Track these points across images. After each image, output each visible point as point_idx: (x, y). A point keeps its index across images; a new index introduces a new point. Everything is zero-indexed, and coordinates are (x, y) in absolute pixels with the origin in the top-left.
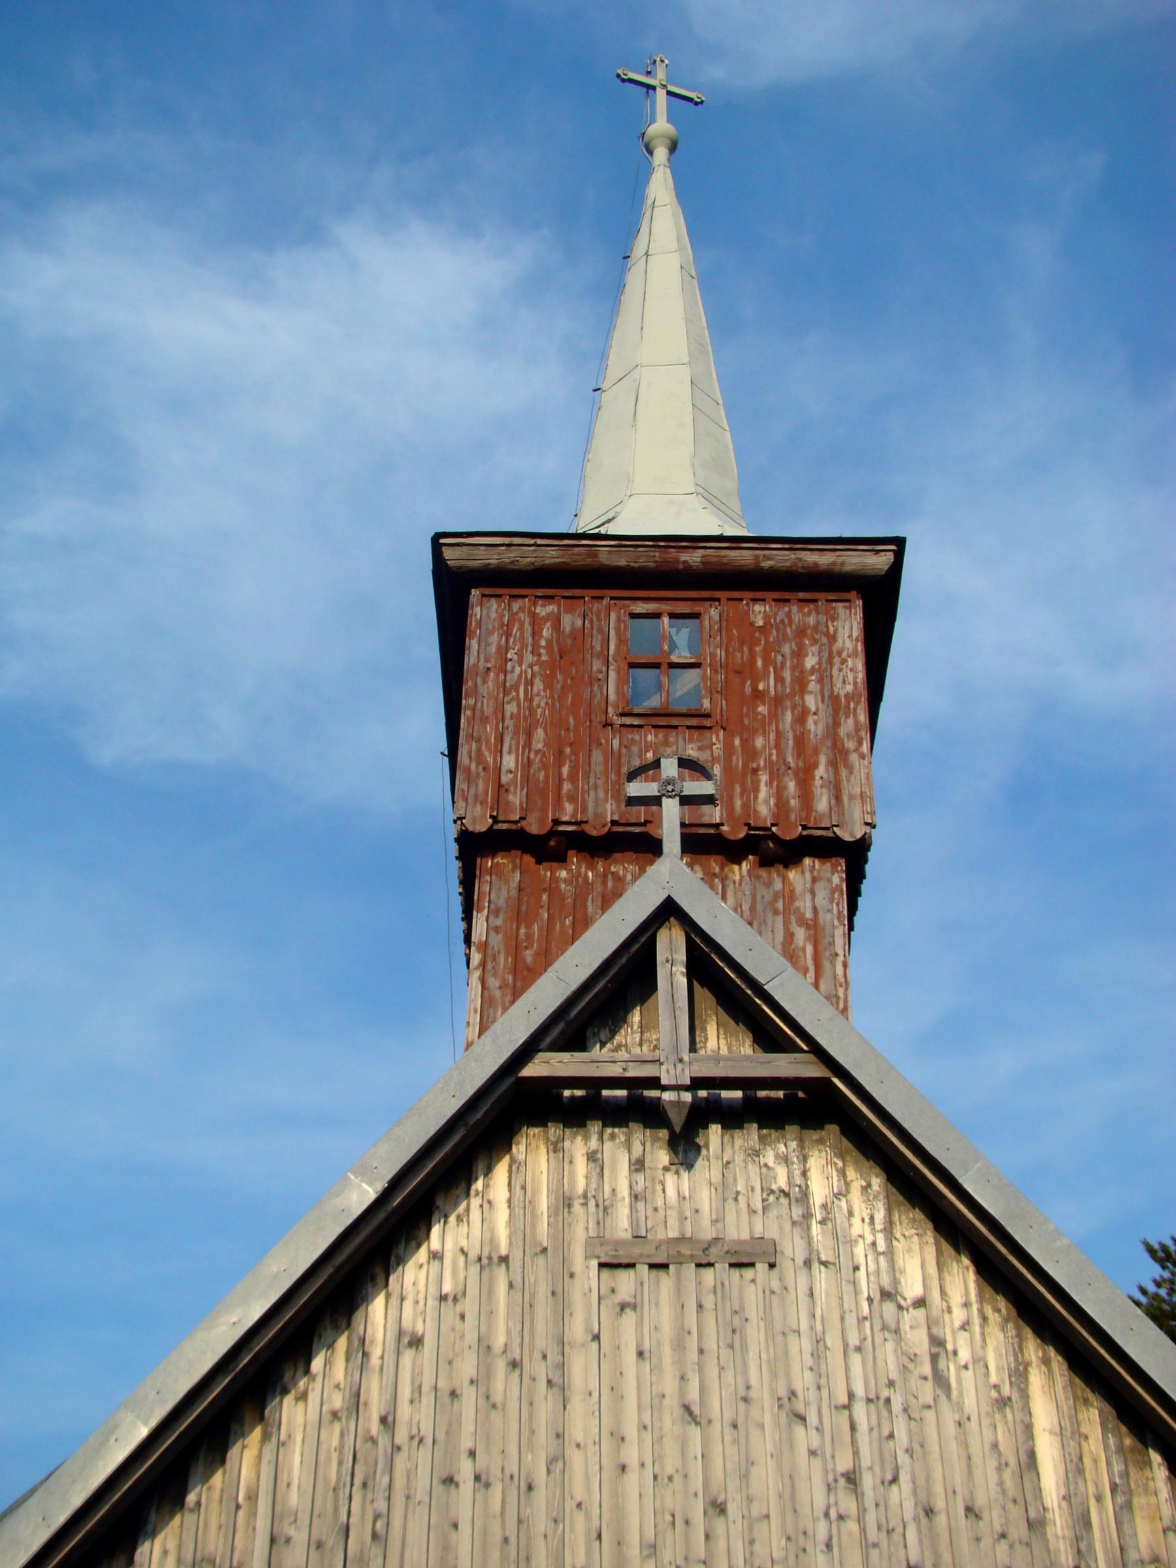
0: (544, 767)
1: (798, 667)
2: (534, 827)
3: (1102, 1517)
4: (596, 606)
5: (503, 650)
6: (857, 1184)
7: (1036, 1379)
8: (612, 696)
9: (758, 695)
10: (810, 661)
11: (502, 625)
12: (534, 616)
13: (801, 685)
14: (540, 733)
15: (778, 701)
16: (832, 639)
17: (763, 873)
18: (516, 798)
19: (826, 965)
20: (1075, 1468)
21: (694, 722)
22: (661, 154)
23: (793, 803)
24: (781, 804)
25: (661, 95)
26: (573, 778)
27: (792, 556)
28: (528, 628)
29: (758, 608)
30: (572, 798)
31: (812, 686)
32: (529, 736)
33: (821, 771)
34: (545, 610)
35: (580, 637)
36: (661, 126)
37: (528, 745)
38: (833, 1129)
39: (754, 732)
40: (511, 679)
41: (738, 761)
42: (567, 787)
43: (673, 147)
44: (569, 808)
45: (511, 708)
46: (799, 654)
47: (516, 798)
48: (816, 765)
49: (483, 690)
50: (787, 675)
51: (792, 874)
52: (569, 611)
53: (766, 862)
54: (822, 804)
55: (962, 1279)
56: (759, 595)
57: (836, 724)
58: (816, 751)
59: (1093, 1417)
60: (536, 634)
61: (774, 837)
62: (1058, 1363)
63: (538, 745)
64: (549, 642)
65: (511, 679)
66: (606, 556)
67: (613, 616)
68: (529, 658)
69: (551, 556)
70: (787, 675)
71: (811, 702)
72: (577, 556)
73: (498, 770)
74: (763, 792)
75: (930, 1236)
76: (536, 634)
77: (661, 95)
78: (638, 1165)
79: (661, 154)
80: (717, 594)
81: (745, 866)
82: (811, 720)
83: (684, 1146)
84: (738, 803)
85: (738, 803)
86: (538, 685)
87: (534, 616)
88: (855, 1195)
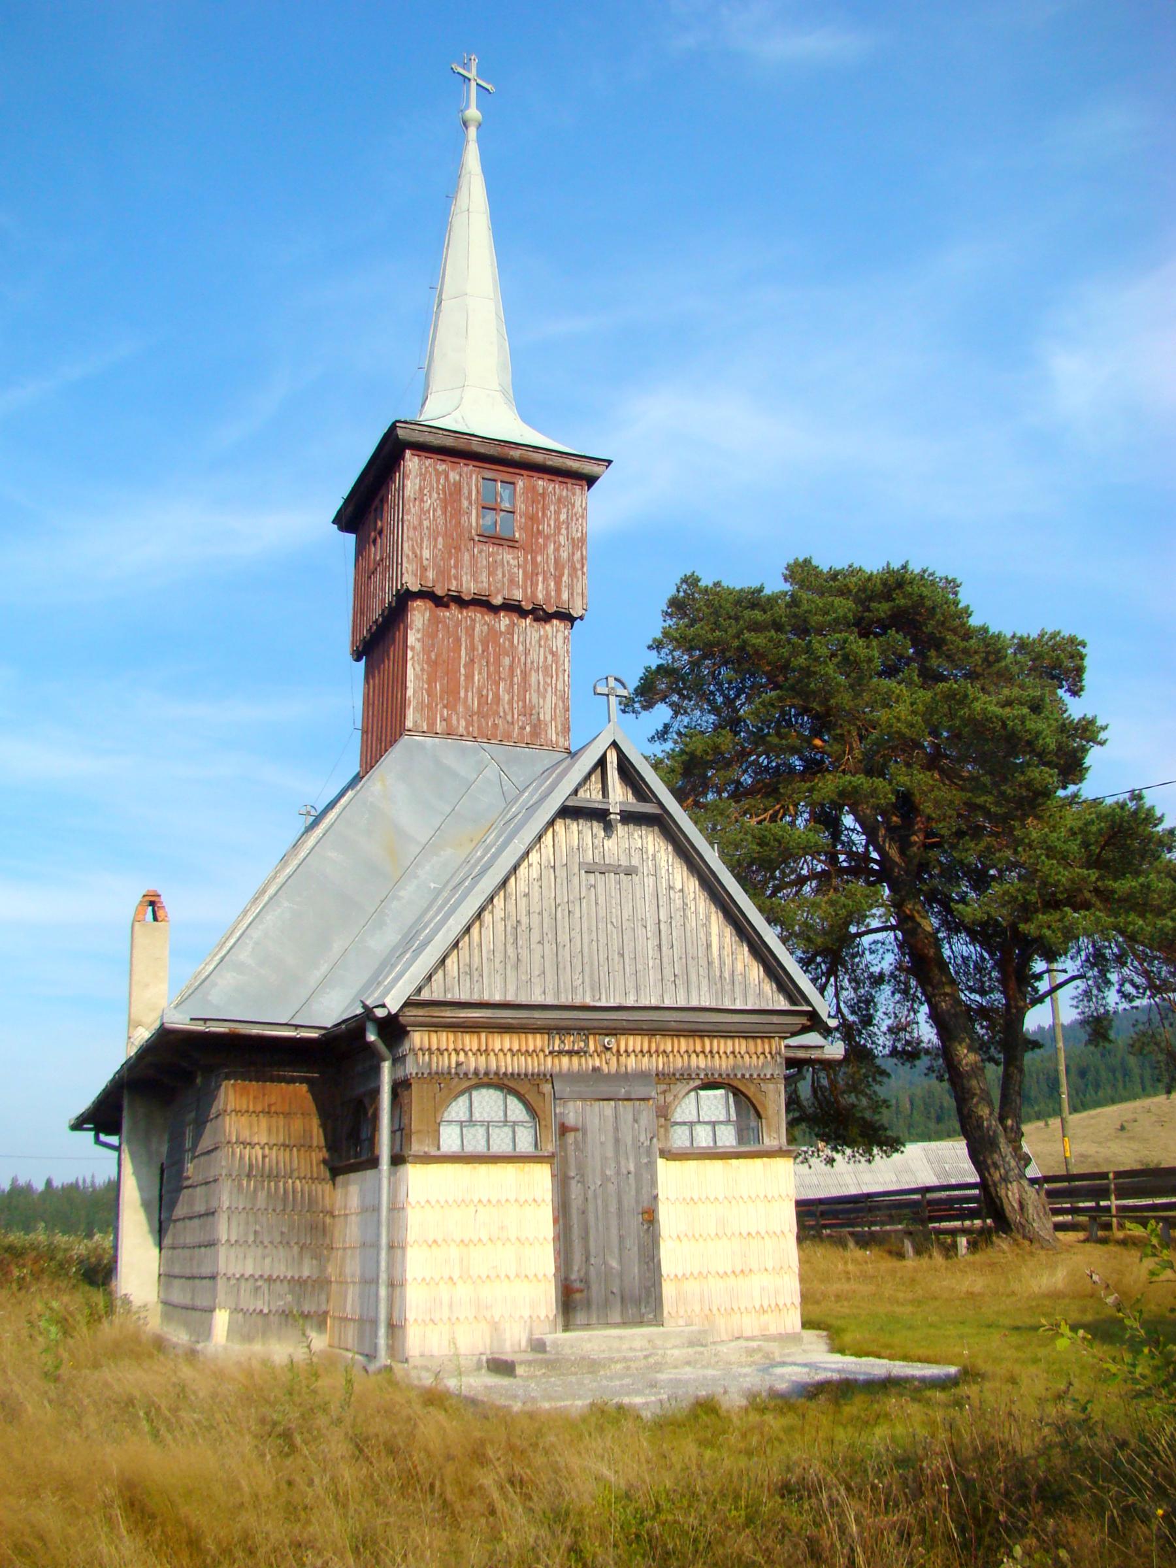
0: (443, 559)
1: (557, 519)
2: (440, 592)
3: (728, 961)
4: (465, 469)
5: (421, 489)
6: (664, 848)
7: (713, 917)
8: (474, 524)
9: (539, 532)
10: (563, 517)
11: (421, 474)
12: (436, 470)
13: (558, 528)
14: (440, 539)
15: (547, 538)
16: (573, 506)
17: (535, 624)
18: (431, 574)
19: (561, 676)
20: (721, 948)
21: (511, 544)
22: (472, 132)
23: (553, 593)
24: (548, 594)
25: (473, 85)
26: (456, 567)
27: (561, 460)
28: (434, 477)
29: (540, 482)
30: (456, 578)
31: (564, 531)
32: (436, 540)
33: (565, 578)
34: (442, 467)
35: (458, 486)
36: (473, 113)
37: (435, 546)
38: (656, 828)
39: (536, 553)
40: (426, 506)
41: (529, 568)
42: (453, 571)
43: (479, 126)
44: (454, 583)
45: (426, 523)
46: (557, 513)
47: (431, 574)
48: (563, 575)
49: (413, 510)
50: (552, 523)
51: (548, 627)
52: (453, 470)
53: (536, 620)
54: (565, 596)
55: (693, 884)
56: (541, 475)
57: (573, 554)
58: (563, 568)
59: (728, 931)
60: (438, 481)
61: (543, 610)
62: (720, 915)
63: (440, 546)
64: (444, 487)
65: (426, 506)
66: (476, 447)
67: (474, 477)
68: (435, 495)
69: (449, 442)
70: (552, 523)
71: (562, 540)
72: (460, 444)
73: (421, 558)
74: (540, 587)
75: (685, 868)
76: (438, 481)
77: (473, 85)
78: (594, 836)
79: (472, 132)
80: (522, 472)
81: (528, 621)
82: (562, 549)
83: (608, 828)
84: (529, 591)
85: (529, 591)
86: (439, 512)
87: (436, 470)
88: (662, 852)
